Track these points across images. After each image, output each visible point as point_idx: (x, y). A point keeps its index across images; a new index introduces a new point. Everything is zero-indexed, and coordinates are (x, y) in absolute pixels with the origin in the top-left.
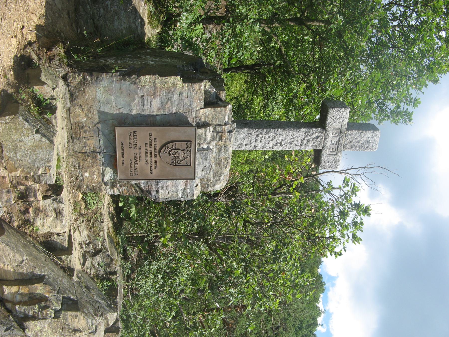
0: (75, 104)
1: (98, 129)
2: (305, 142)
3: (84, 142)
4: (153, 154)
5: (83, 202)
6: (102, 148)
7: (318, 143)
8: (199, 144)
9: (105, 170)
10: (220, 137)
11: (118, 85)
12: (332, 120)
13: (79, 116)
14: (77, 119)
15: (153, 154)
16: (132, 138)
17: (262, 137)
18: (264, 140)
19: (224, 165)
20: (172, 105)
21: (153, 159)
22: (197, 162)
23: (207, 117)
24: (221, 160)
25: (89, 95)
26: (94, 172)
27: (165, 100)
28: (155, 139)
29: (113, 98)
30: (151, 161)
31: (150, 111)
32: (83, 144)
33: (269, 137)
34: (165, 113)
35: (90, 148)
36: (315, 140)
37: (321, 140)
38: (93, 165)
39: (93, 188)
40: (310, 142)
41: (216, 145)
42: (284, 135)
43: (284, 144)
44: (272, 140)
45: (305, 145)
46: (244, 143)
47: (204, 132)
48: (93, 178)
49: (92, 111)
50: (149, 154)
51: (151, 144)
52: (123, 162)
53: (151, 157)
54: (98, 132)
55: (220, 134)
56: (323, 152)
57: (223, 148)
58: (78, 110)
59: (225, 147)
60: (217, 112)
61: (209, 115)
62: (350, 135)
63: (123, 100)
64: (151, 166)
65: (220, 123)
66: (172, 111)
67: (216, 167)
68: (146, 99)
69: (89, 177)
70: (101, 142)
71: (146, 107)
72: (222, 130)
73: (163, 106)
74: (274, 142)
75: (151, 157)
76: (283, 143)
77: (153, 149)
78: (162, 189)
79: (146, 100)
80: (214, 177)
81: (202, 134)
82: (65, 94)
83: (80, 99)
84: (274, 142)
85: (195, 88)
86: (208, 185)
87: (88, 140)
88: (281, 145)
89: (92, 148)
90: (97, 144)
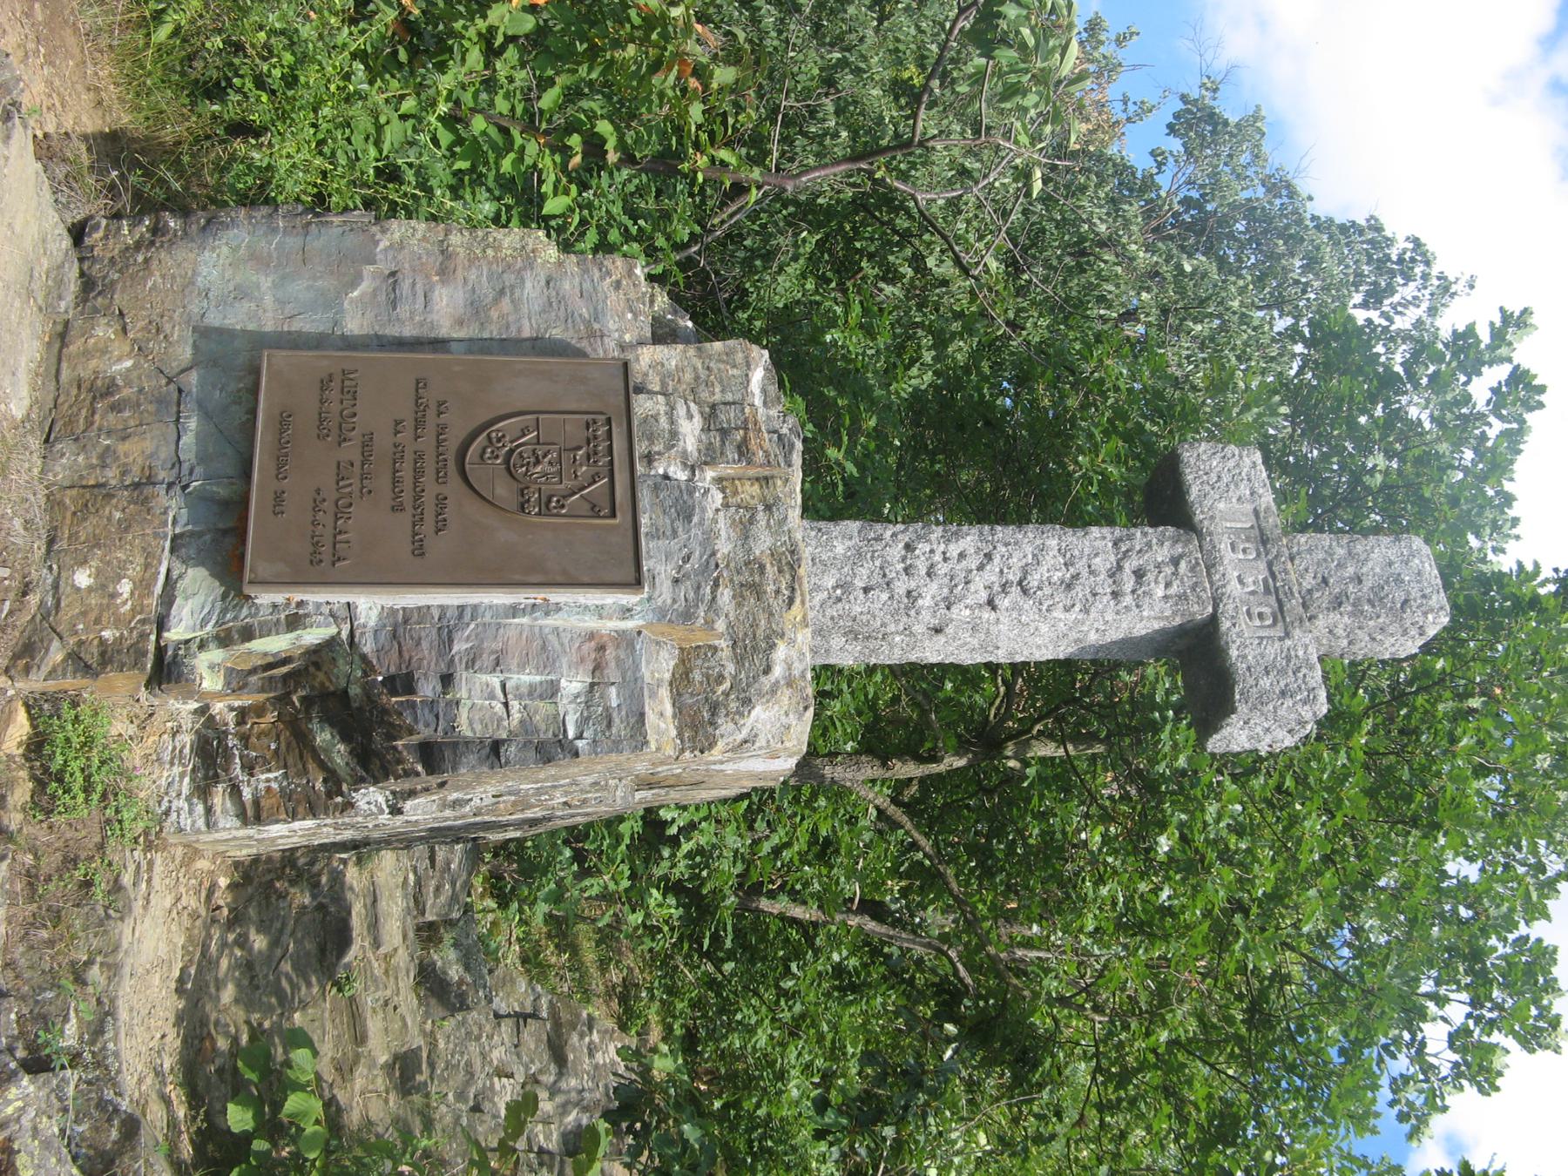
0: (96, 310)
1: (180, 391)
2: (1129, 583)
3: (99, 450)
4: (430, 466)
5: (24, 774)
6: (186, 466)
7: (1188, 582)
8: (649, 459)
9: (180, 577)
10: (739, 447)
11: (293, 242)
12: (1207, 488)
13: (104, 351)
14: (93, 363)
15: (430, 466)
16: (334, 394)
17: (932, 551)
18: (942, 569)
19: (778, 592)
20: (517, 309)
21: (431, 489)
22: (644, 520)
23: (670, 375)
24: (762, 568)
25: (163, 277)
26: (123, 565)
27: (486, 291)
28: (440, 404)
29: (266, 282)
30: (417, 497)
31: (421, 324)
32: (94, 454)
33: (962, 556)
34: (486, 335)
35: (123, 474)
36: (1168, 570)
37: (1192, 569)
38: (126, 530)
39: (103, 654)
40: (1150, 577)
41: (726, 506)
42: (1029, 549)
43: (1040, 588)
44: (981, 568)
45: (1133, 592)
46: (859, 584)
47: (662, 409)
48: (114, 595)
49: (167, 327)
50: (406, 473)
51: (419, 423)
52: (279, 498)
53: (418, 473)
54: (179, 405)
55: (739, 435)
56: (1225, 625)
57: (761, 516)
58: (104, 331)
59: (768, 508)
60: (710, 357)
61: (678, 369)
62: (1310, 551)
63: (309, 288)
64: (418, 520)
65: (729, 397)
66: (519, 330)
67: (739, 605)
68: (408, 282)
69: (90, 589)
70: (188, 439)
71: (403, 310)
72: (746, 420)
73: (476, 309)
74: (991, 575)
75: (418, 473)
76: (1033, 581)
77: (427, 442)
78: (471, 664)
79: (405, 286)
80: (739, 661)
81: (656, 418)
82: (61, 266)
83: (123, 292)
84: (991, 575)
85: (611, 267)
86: (714, 708)
87: (124, 439)
88: (1025, 592)
89: (136, 469)
90: (166, 452)
